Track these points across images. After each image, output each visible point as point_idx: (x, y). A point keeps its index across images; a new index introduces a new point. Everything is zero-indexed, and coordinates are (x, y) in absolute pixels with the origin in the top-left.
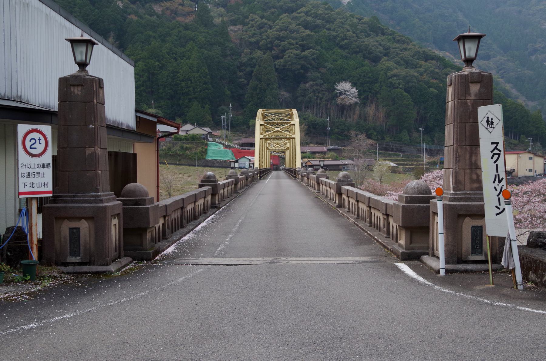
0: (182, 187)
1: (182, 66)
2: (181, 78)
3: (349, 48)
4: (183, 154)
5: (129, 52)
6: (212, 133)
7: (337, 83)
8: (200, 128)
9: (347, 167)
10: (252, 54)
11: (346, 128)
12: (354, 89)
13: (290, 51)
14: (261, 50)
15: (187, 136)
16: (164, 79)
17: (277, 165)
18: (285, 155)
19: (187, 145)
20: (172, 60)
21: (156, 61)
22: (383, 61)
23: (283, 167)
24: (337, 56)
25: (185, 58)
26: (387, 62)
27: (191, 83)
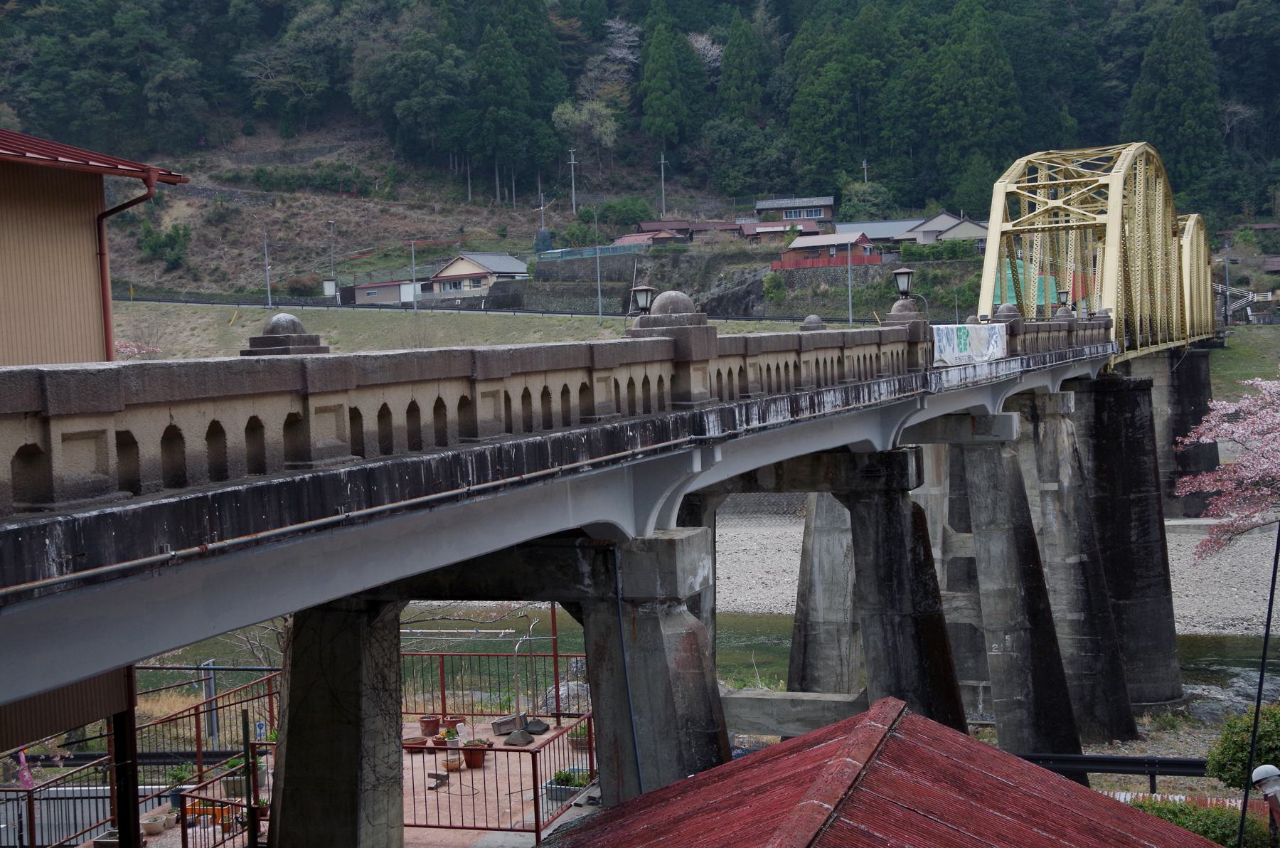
1: (940, 61)
2: (938, 94)
16: (894, 103)
19: (939, 272)
20: (915, 48)
21: (872, 58)
25: (948, 41)
27: (966, 105)
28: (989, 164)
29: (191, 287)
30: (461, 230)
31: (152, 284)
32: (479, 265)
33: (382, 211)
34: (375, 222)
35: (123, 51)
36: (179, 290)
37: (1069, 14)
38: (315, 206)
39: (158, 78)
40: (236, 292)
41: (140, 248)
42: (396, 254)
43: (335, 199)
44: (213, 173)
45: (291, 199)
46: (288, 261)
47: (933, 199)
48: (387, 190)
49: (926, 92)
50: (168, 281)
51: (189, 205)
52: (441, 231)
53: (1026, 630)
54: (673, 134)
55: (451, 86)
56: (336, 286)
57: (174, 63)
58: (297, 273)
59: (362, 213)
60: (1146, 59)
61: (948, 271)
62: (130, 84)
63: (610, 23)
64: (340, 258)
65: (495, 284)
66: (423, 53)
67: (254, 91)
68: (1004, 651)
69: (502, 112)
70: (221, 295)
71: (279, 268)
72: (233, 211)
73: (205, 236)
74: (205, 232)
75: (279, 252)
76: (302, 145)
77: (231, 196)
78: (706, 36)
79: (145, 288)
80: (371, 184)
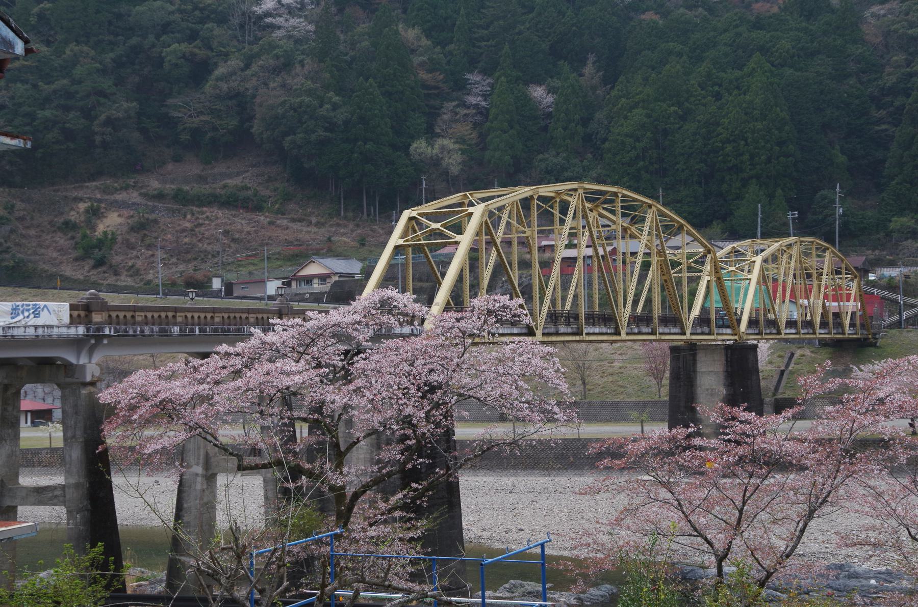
0: (620, 368)
1: (728, 108)
2: (724, 135)
5: (618, 90)
10: (913, 64)
16: (687, 142)
20: (709, 98)
21: (673, 105)
29: (111, 280)
30: (329, 239)
31: (82, 277)
32: (326, 267)
33: (270, 223)
34: (263, 232)
35: (78, 96)
36: (102, 282)
37: (848, 70)
38: (217, 218)
39: (103, 117)
40: (145, 284)
41: (75, 248)
42: (275, 257)
43: (234, 212)
44: (143, 191)
45: (199, 212)
46: (189, 261)
48: (277, 206)
50: (94, 275)
51: (119, 216)
52: (314, 240)
53: (87, 510)
54: (509, 165)
55: (327, 125)
56: (222, 281)
57: (117, 105)
58: (195, 270)
59: (252, 225)
60: (907, 107)
62: (82, 121)
63: (468, 76)
64: (231, 260)
65: (335, 282)
66: (307, 99)
67: (180, 127)
68: (76, 525)
69: (368, 146)
70: (133, 286)
71: (181, 266)
72: (152, 221)
73: (127, 240)
74: (128, 237)
75: (180, 253)
76: (216, 171)
77: (153, 210)
78: (543, 87)
79: (76, 280)
80: (265, 202)
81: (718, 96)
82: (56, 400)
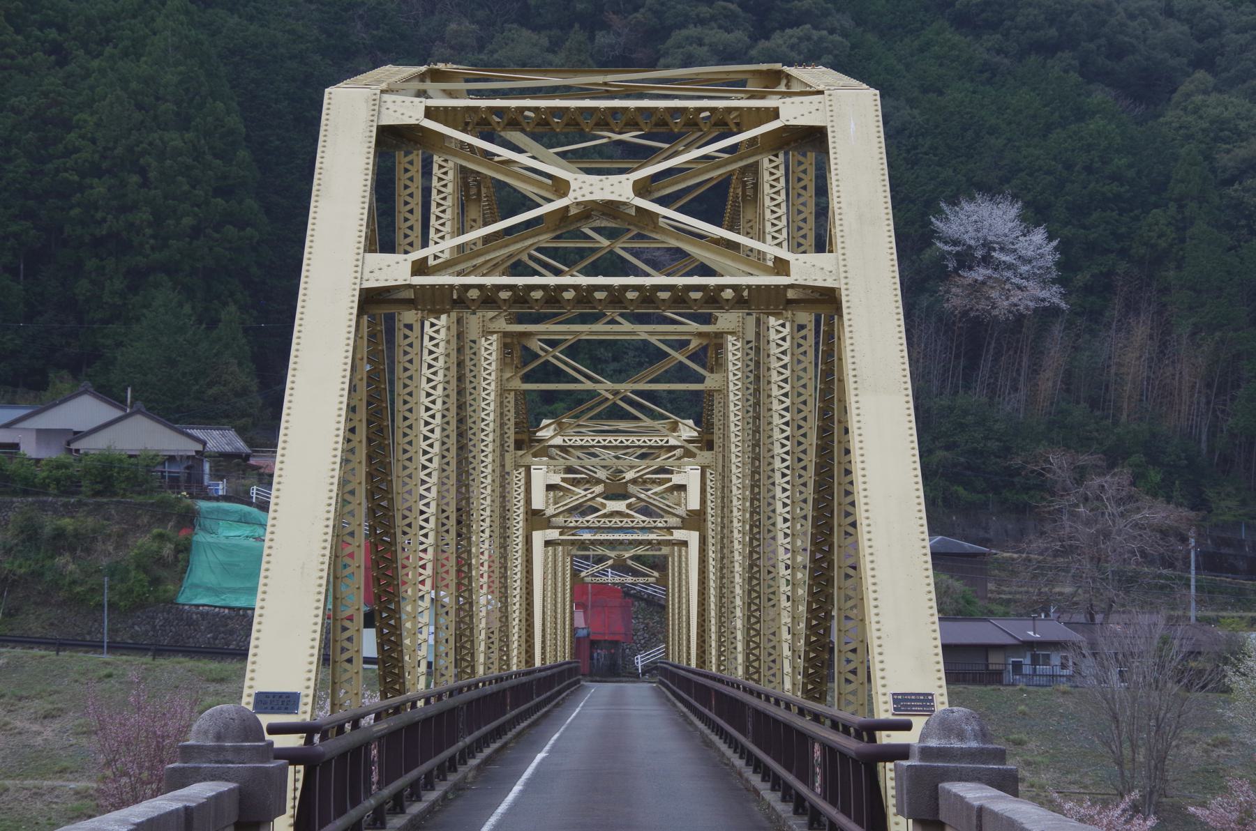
1: (92, 88)
3: (1008, 23)
4: (37, 575)
6: (248, 457)
7: (942, 204)
8: (176, 430)
9: (1035, 661)
11: (994, 445)
12: (1038, 236)
13: (692, 31)
14: (536, 29)
15: (66, 466)
17: (615, 643)
18: (663, 581)
19: (67, 522)
20: (39, 55)
22: (1188, 95)
23: (655, 654)
24: (941, 65)
25: (109, 50)
26: (1213, 98)
27: (145, 183)
28: (187, 309)
47: (65, 373)
49: (60, 147)
61: (90, 522)
81: (60, 55)
82: (1130, 757)
